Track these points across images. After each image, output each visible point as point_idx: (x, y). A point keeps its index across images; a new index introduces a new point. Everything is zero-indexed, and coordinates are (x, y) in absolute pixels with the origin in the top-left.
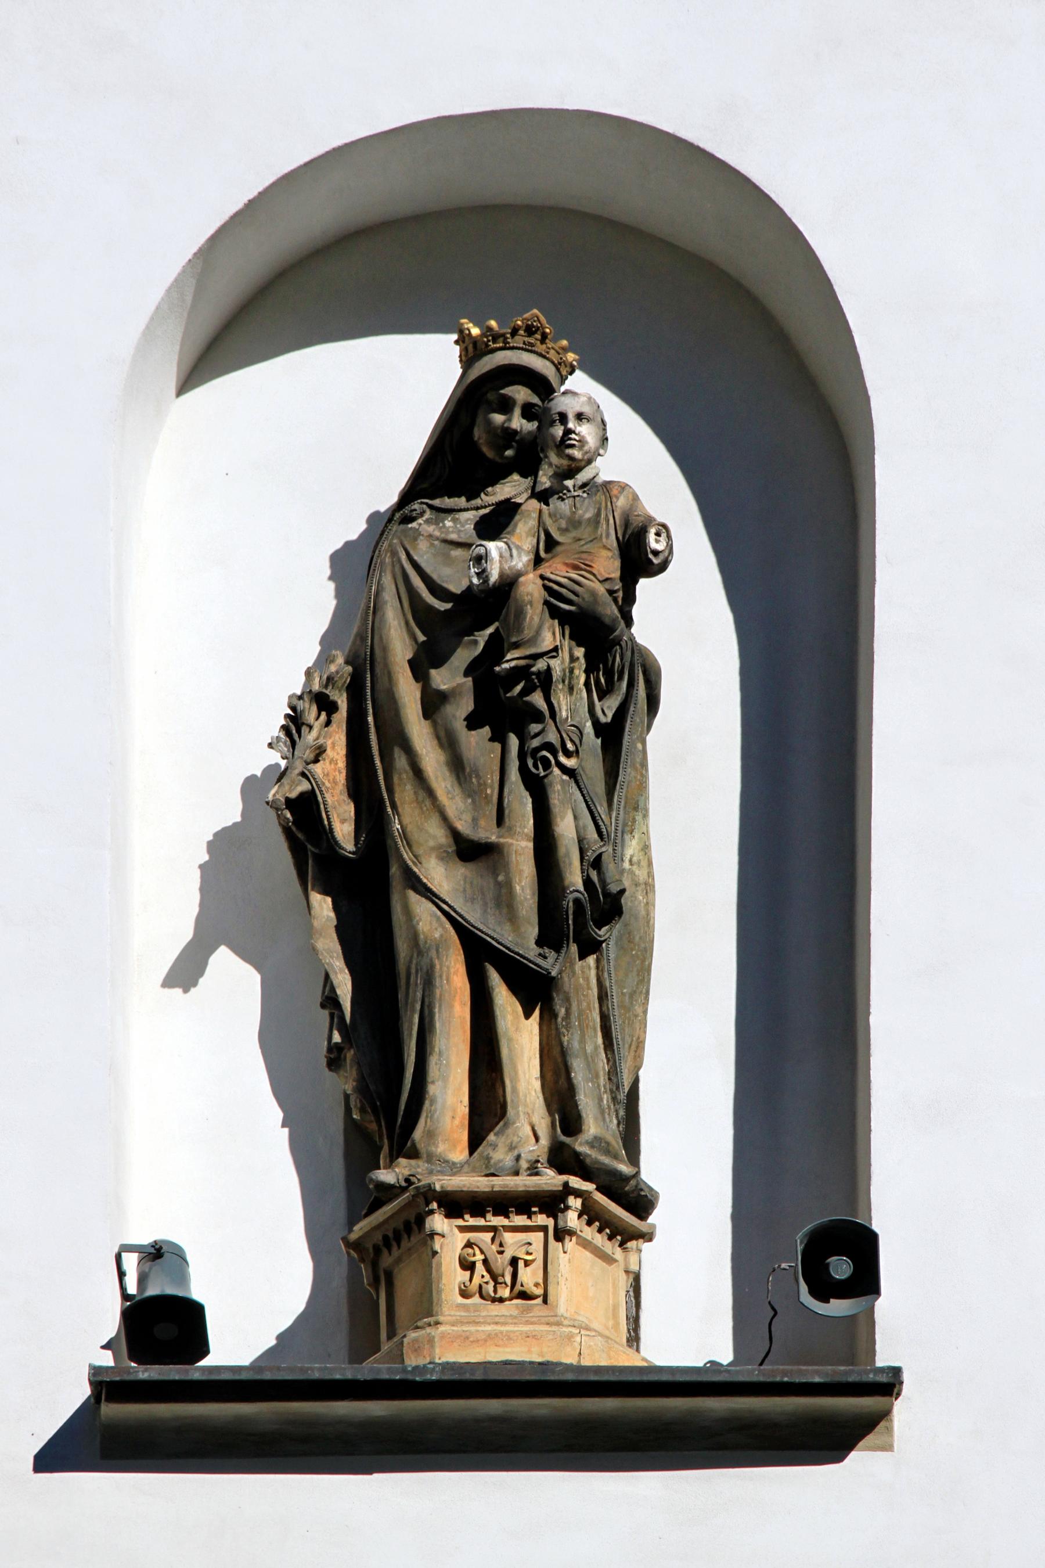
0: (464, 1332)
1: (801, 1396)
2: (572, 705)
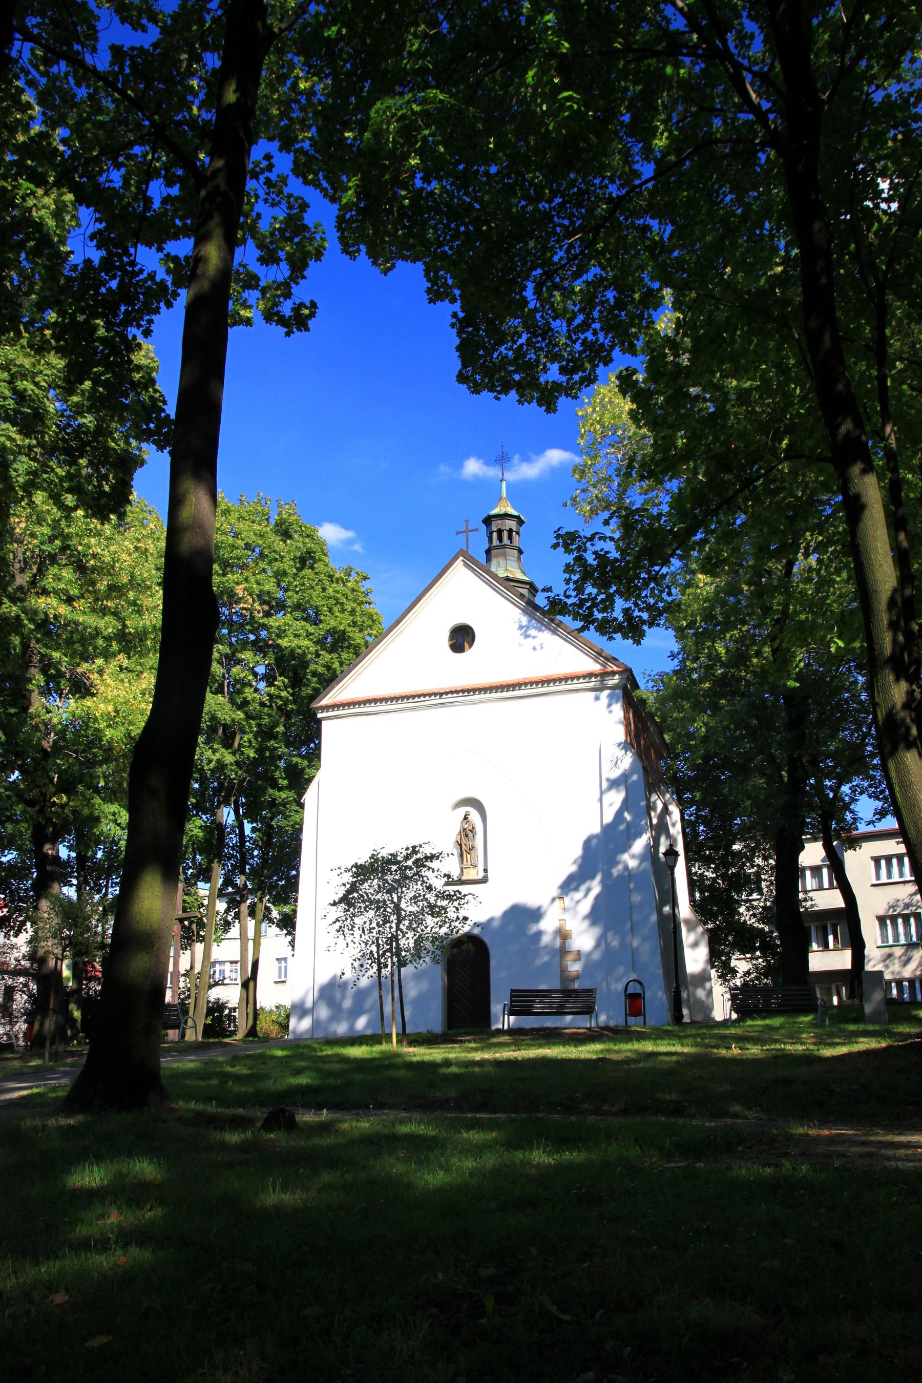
0: (464, 878)
1: (484, 880)
2: (471, 835)
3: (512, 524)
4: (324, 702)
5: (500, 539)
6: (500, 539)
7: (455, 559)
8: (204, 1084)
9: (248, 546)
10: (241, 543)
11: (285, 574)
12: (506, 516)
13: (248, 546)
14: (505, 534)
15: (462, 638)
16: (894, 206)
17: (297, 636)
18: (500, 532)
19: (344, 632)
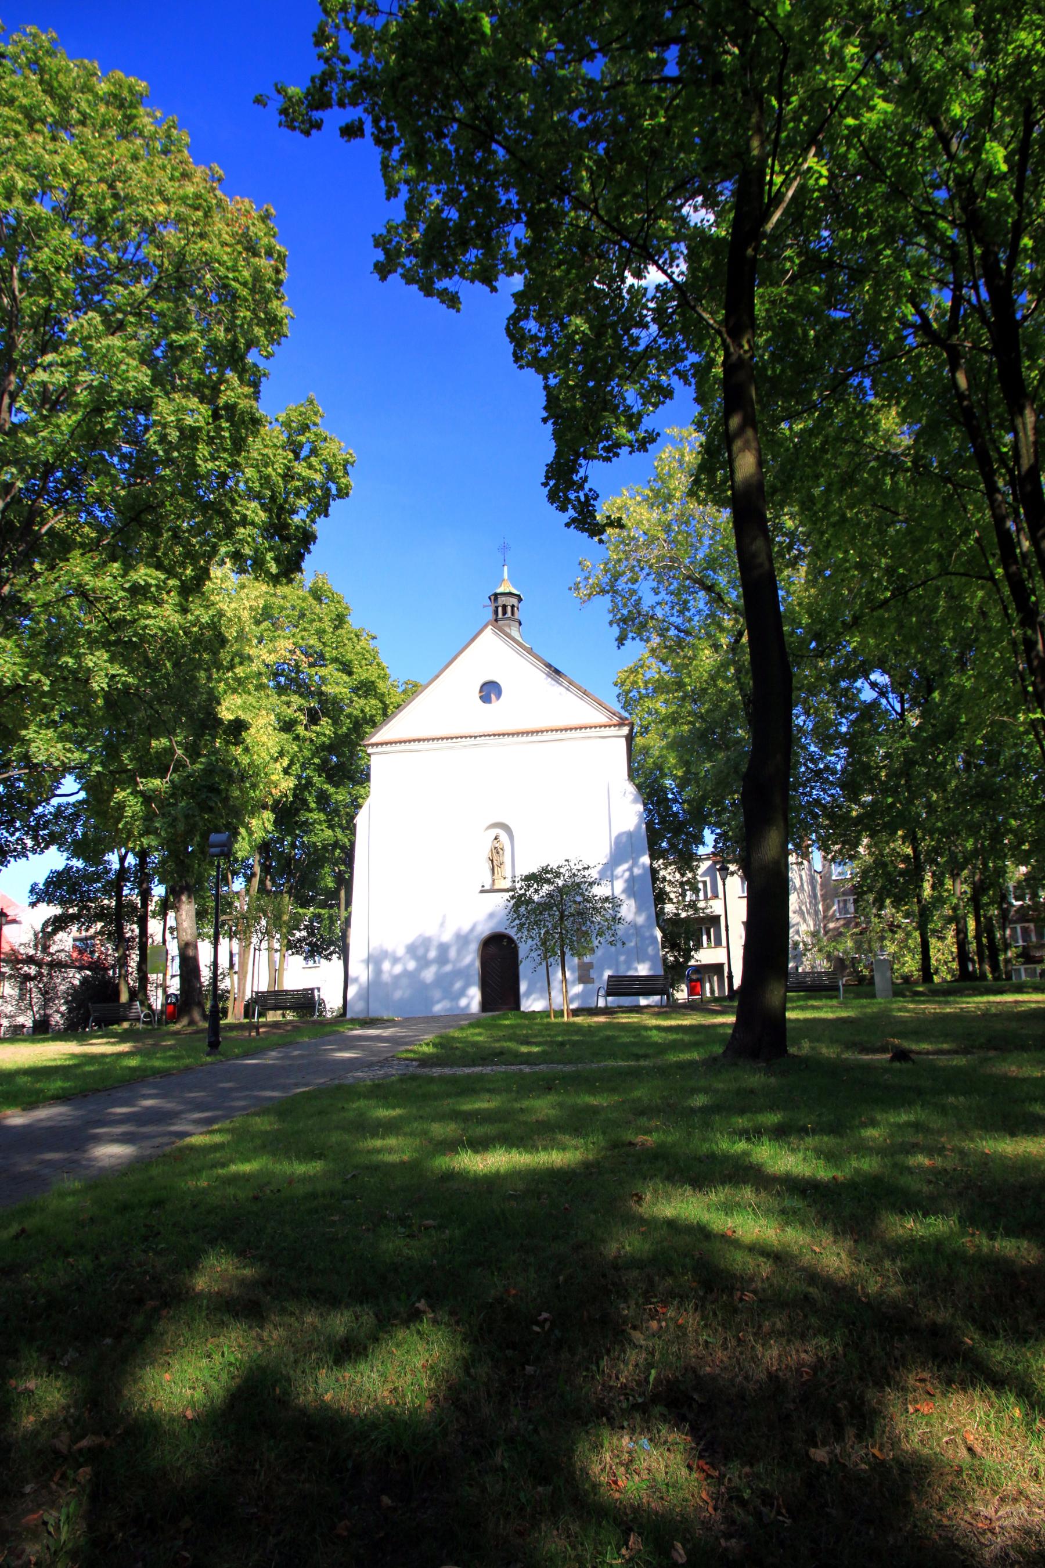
0: (496, 887)
3: (514, 601)
4: (374, 740)
5: (504, 613)
6: (504, 613)
7: (486, 626)
8: (940, 1046)
9: (294, 608)
10: (288, 605)
11: (324, 631)
12: (510, 594)
13: (294, 608)
14: (509, 609)
15: (490, 691)
16: (123, 493)
17: (338, 684)
18: (504, 607)
19: (373, 682)
